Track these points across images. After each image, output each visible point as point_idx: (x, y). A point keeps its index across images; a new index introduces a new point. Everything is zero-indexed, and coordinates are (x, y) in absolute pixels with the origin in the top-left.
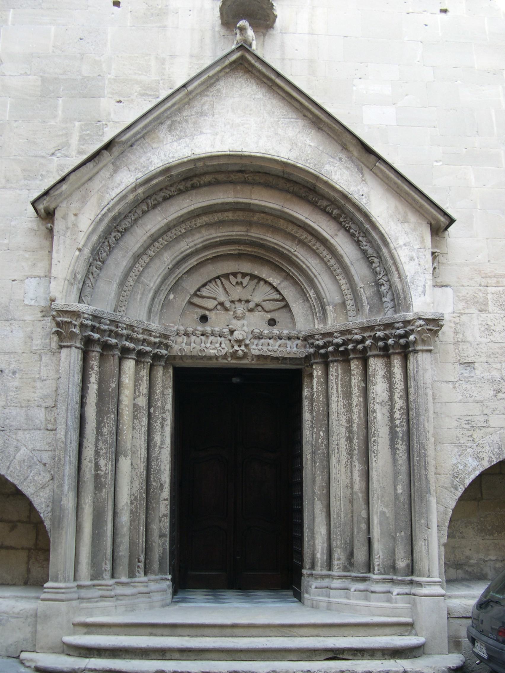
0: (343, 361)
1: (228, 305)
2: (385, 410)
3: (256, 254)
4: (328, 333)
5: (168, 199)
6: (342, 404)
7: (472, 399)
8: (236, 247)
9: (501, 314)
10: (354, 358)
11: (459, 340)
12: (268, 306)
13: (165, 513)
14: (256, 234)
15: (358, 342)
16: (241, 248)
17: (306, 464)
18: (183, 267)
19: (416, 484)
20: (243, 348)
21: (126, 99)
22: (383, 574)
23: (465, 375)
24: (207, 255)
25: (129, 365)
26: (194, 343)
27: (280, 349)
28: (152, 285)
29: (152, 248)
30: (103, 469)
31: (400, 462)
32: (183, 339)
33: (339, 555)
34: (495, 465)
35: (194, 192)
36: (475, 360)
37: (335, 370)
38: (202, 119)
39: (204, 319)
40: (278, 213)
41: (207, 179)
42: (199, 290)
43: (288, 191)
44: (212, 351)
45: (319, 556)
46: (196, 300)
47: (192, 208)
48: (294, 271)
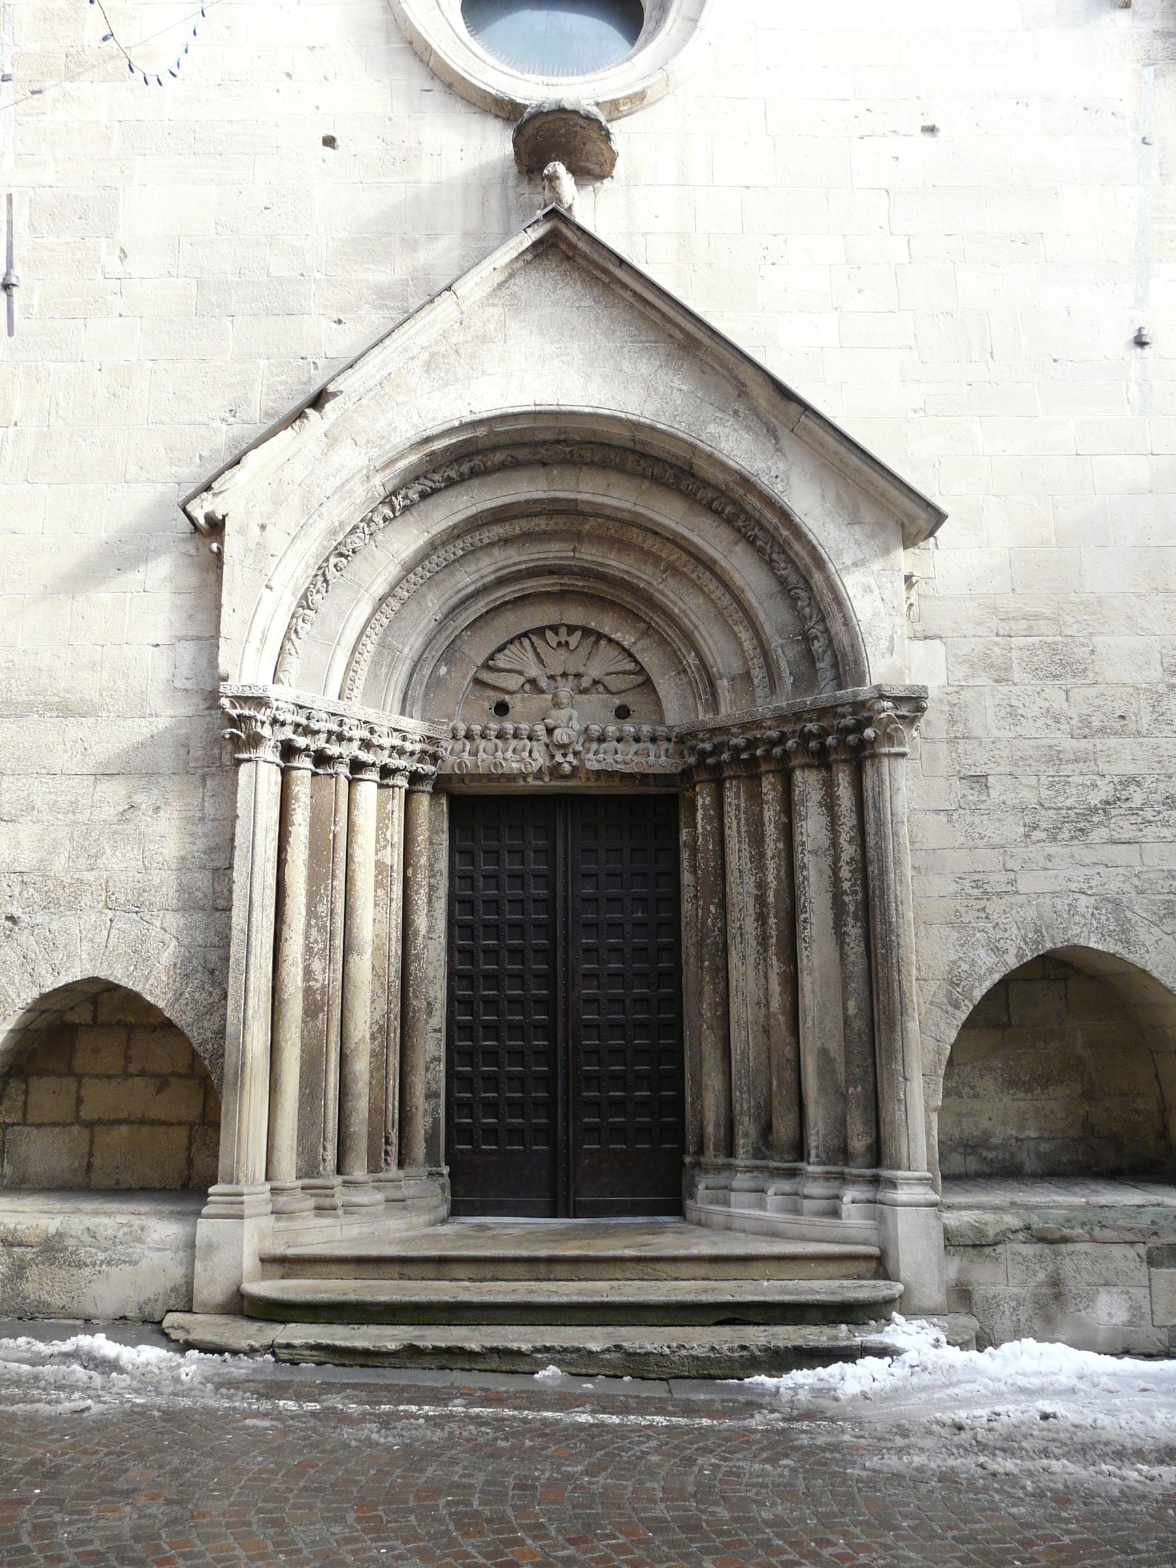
0: (749, 777)
1: (543, 683)
2: (826, 862)
3: (591, 591)
4: (719, 729)
5: (430, 495)
6: (748, 855)
7: (983, 842)
8: (554, 580)
9: (1037, 685)
10: (767, 772)
11: (958, 735)
12: (614, 683)
13: (436, 1054)
14: (590, 554)
15: (773, 743)
16: (566, 580)
17: (687, 964)
18: (462, 618)
19: (882, 998)
20: (570, 758)
21: (348, 316)
22: (825, 1164)
23: (970, 797)
24: (504, 596)
25: (368, 791)
26: (484, 751)
27: (636, 759)
28: (406, 650)
29: (404, 584)
30: (319, 977)
31: (852, 958)
32: (464, 744)
33: (747, 1131)
34: (1028, 962)
35: (476, 482)
36: (989, 772)
37: (734, 798)
38: (485, 347)
39: (502, 709)
40: (626, 516)
41: (499, 457)
42: (491, 657)
43: (643, 476)
44: (515, 765)
45: (710, 1129)
46: (487, 676)
47: (473, 511)
48: (658, 620)
